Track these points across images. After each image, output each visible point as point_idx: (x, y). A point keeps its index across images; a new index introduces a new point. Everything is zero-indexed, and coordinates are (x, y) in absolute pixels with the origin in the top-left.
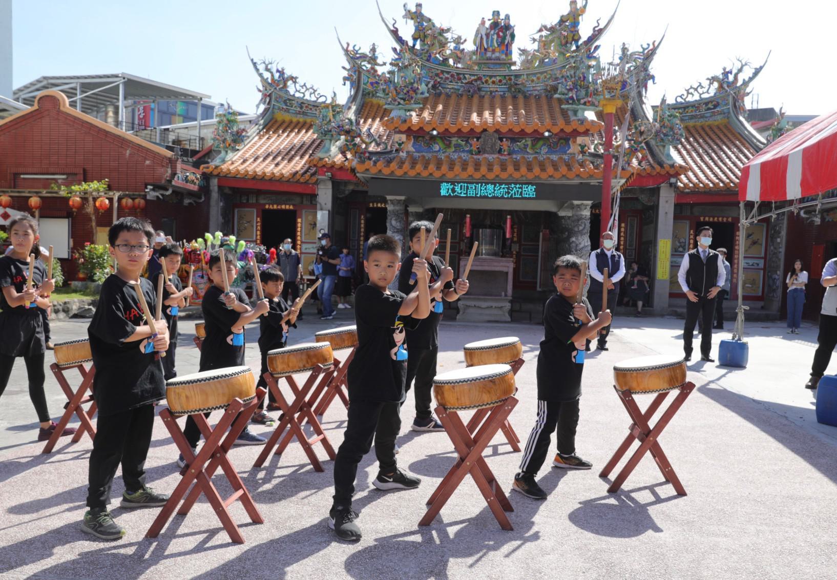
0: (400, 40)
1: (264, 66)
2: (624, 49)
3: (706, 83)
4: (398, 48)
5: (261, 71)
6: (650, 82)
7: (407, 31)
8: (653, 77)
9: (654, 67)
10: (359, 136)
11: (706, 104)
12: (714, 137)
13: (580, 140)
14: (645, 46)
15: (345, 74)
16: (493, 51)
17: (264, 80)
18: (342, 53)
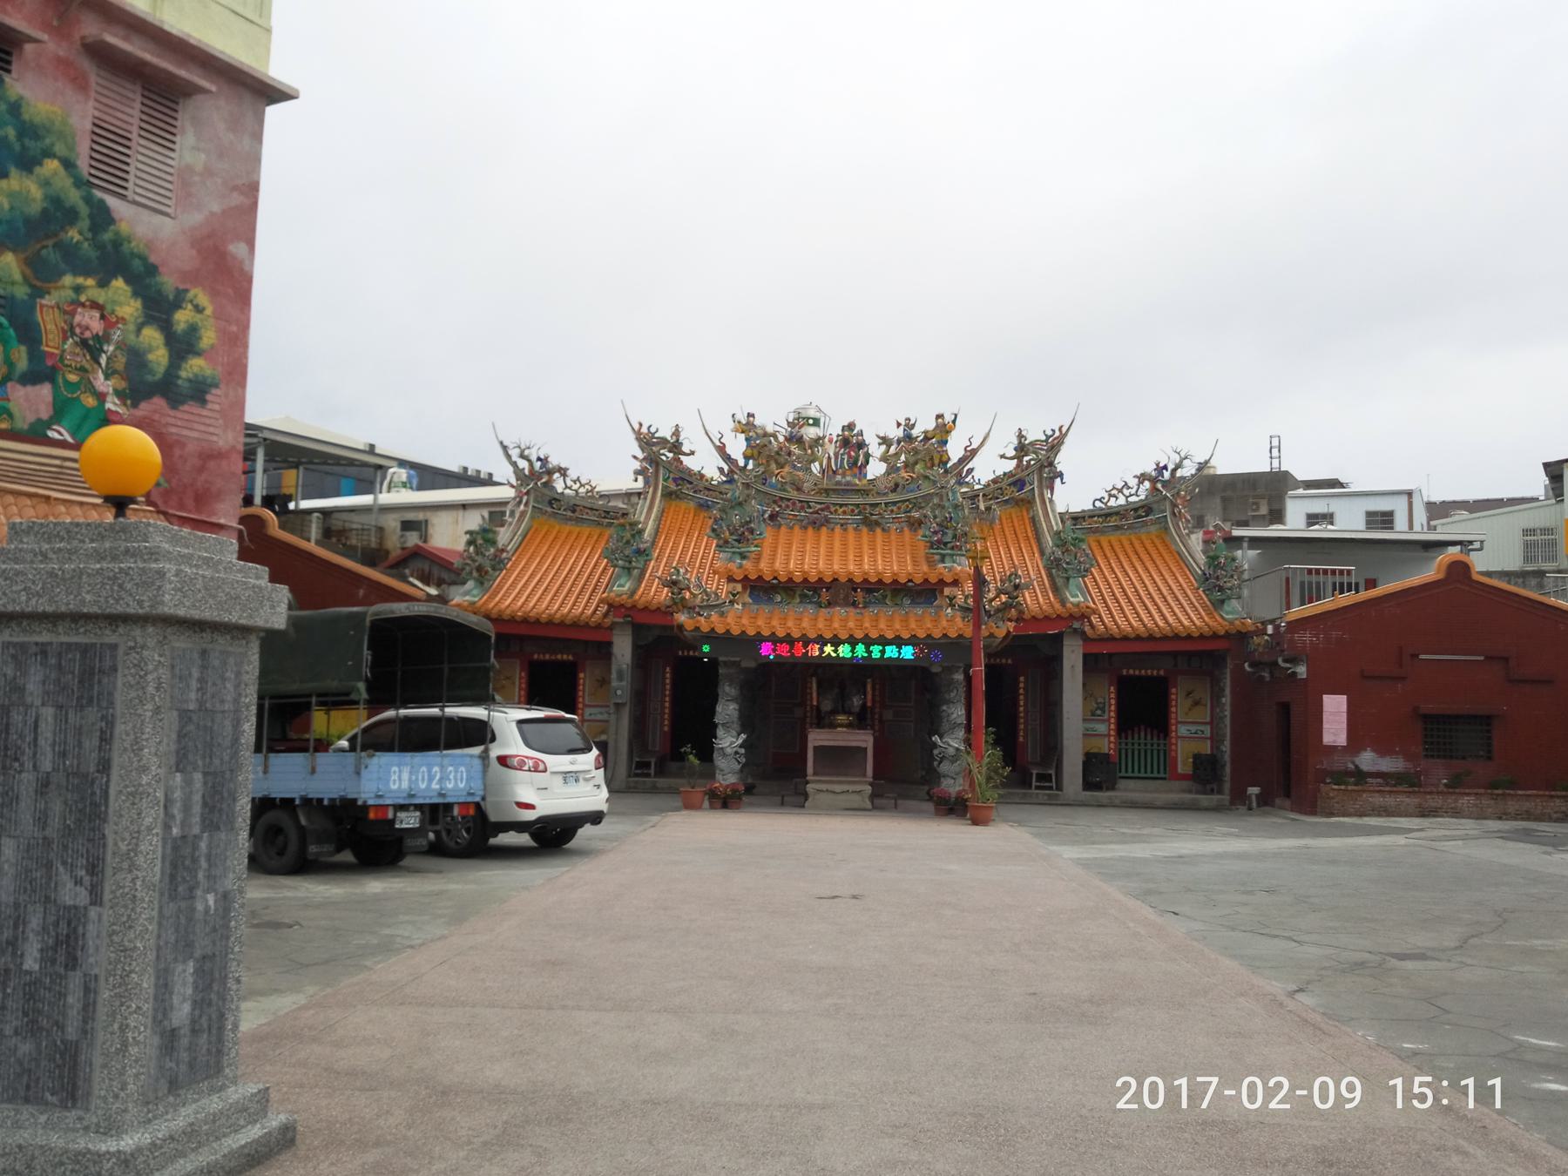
0: (727, 458)
1: (517, 451)
2: (1021, 436)
3: (1133, 482)
4: (726, 468)
5: (515, 458)
6: (1058, 481)
7: (737, 447)
8: (1061, 475)
9: (1063, 461)
10: (688, 589)
11: (1136, 510)
12: (1145, 557)
13: (947, 591)
14: (1049, 433)
15: (637, 465)
16: (844, 475)
17: (518, 472)
18: (633, 436)
